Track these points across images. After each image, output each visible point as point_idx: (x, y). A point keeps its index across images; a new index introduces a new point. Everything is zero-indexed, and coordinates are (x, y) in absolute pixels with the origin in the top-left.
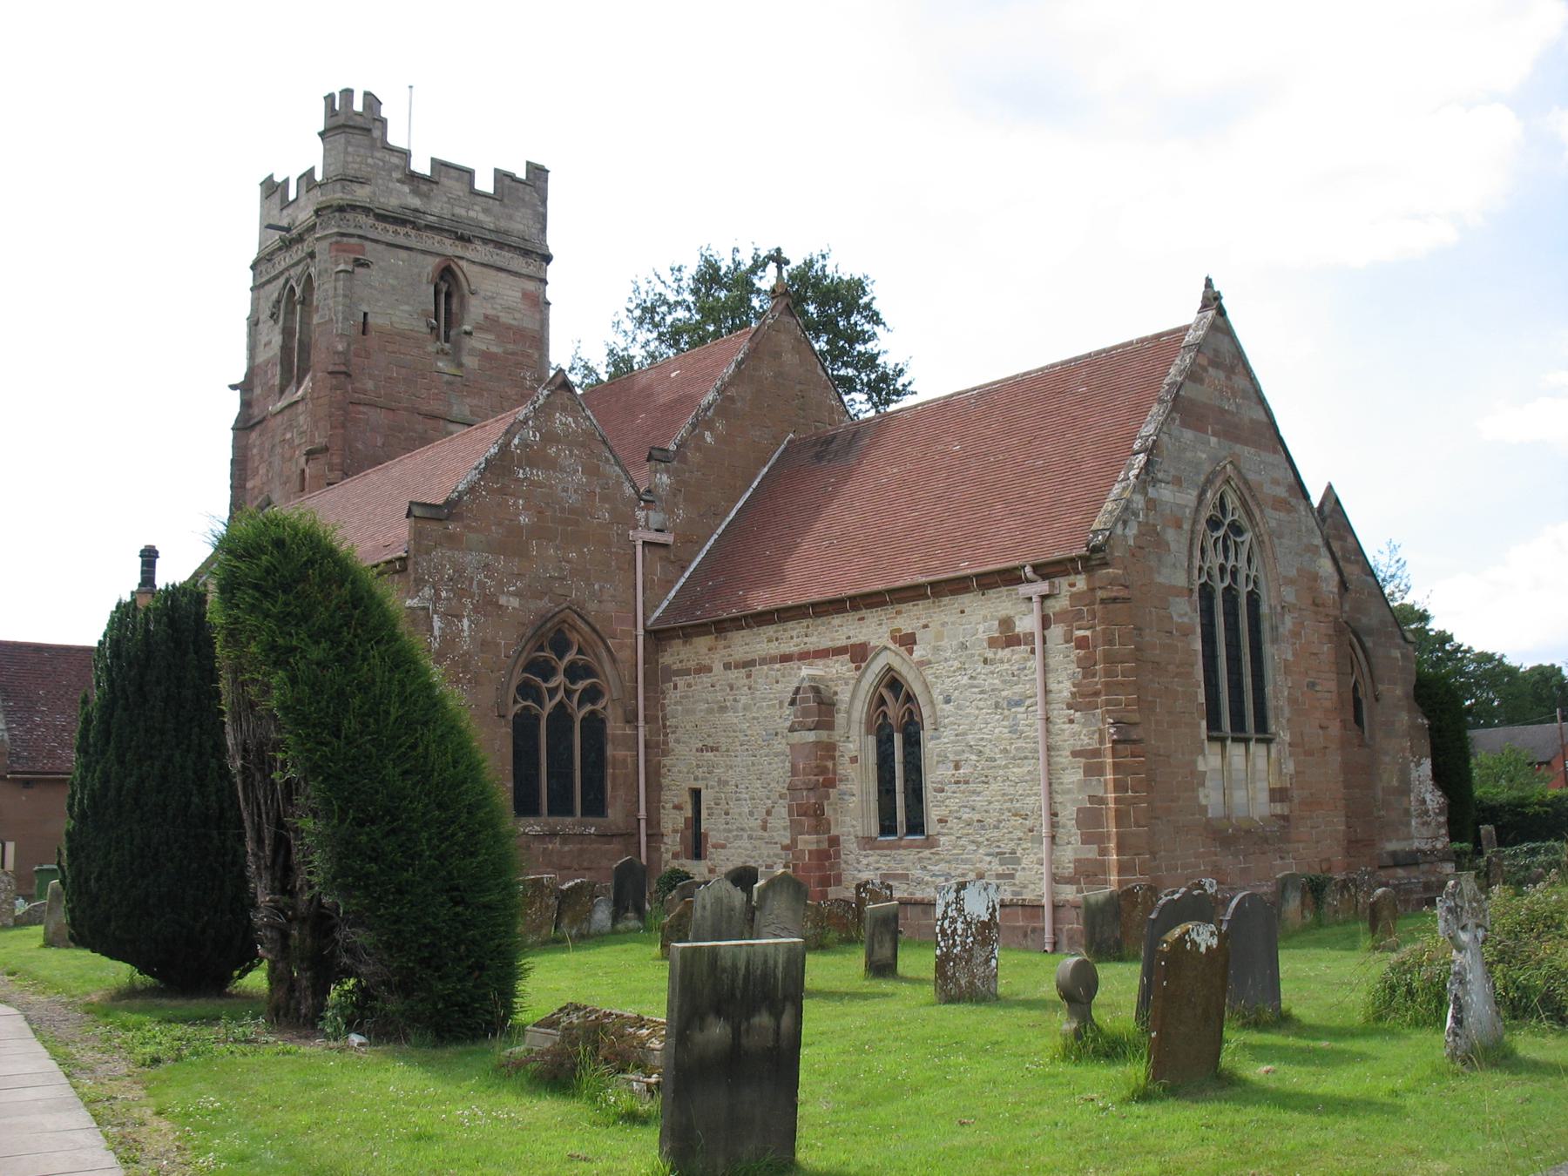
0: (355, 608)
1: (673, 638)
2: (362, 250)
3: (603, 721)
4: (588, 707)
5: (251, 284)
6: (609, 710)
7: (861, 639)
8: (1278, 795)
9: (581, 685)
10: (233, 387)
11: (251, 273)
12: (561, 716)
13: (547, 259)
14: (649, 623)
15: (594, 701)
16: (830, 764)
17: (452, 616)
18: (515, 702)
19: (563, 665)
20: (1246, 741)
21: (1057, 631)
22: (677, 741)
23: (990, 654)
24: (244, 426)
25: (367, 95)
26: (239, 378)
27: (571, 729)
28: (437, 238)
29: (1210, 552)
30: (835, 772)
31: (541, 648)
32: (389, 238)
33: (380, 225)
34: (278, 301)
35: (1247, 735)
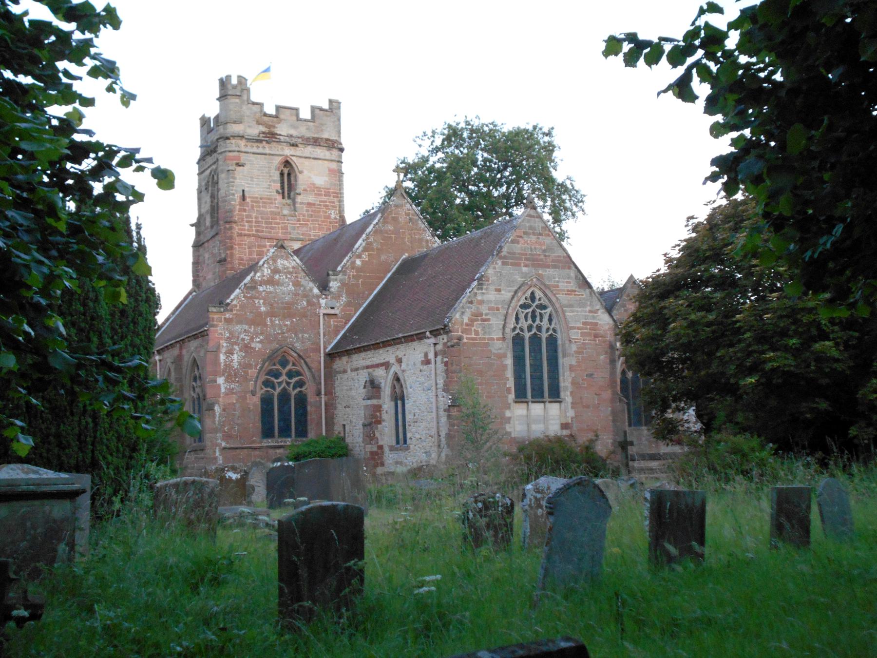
0: (736, 229)
1: (335, 357)
2: (239, 158)
3: (305, 395)
4: (299, 389)
5: (197, 172)
6: (309, 390)
7: (387, 360)
8: (564, 426)
9: (294, 380)
10: (192, 225)
11: (197, 166)
12: (284, 397)
13: (342, 150)
14: (327, 350)
15: (301, 387)
16: (378, 414)
17: (230, 352)
18: (262, 389)
19: (284, 371)
20: (527, 402)
21: (439, 358)
22: (339, 403)
23: (421, 368)
24: (197, 246)
25: (239, 77)
26: (194, 221)
27: (290, 400)
28: (280, 147)
29: (522, 319)
30: (381, 417)
31: (274, 365)
32: (255, 150)
33: (249, 144)
34: (208, 182)
35: (544, 400)
